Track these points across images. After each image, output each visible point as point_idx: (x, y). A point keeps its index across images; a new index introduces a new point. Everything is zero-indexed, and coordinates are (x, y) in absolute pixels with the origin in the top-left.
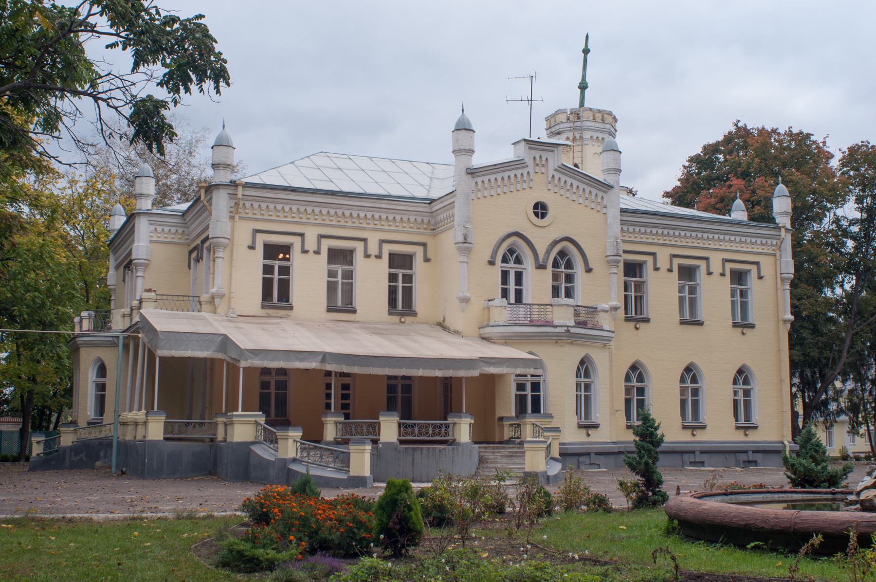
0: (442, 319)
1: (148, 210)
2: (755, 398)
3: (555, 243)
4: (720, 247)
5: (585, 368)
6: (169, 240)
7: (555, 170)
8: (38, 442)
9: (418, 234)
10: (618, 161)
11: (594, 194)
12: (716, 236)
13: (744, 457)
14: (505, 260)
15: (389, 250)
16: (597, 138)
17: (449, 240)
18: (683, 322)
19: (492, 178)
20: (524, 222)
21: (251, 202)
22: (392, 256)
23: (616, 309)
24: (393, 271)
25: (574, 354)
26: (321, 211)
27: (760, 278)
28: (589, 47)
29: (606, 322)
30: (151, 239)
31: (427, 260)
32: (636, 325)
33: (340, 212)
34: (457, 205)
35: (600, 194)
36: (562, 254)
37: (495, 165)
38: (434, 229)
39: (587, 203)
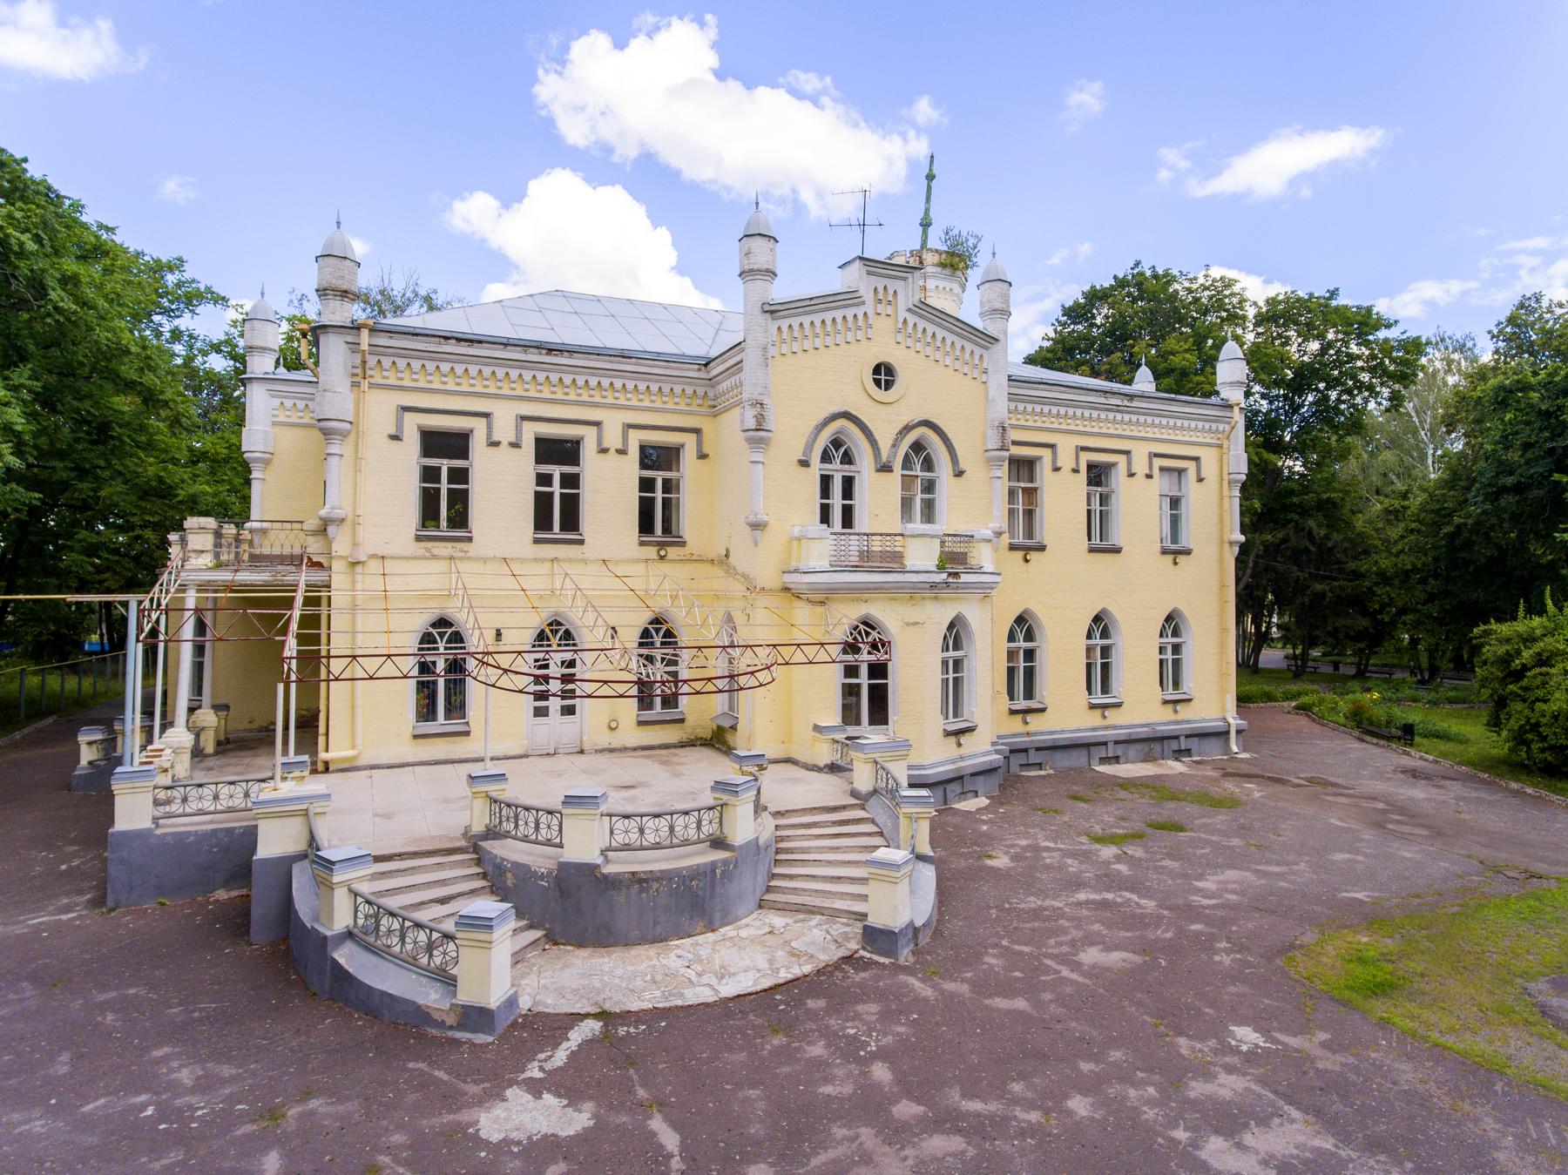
0: (724, 553)
1: (266, 373)
2: (1187, 656)
3: (907, 429)
4: (1123, 433)
5: (956, 634)
6: (294, 420)
7: (909, 310)
8: (90, 743)
9: (681, 412)
10: (1006, 299)
11: (968, 351)
12: (1142, 419)
13: (1174, 745)
14: (826, 457)
15: (640, 441)
16: (944, 288)
17: (729, 430)
18: (1092, 550)
19: (806, 320)
20: (857, 395)
21: (392, 359)
22: (643, 449)
23: (999, 534)
24: (648, 473)
25: (938, 615)
26: (520, 375)
27: (1200, 480)
28: (935, 171)
29: (984, 557)
30: (275, 419)
31: (702, 456)
32: (1025, 555)
33: (554, 377)
34: (747, 365)
35: (978, 351)
36: (918, 447)
37: (811, 299)
38: (715, 407)
39: (958, 365)
